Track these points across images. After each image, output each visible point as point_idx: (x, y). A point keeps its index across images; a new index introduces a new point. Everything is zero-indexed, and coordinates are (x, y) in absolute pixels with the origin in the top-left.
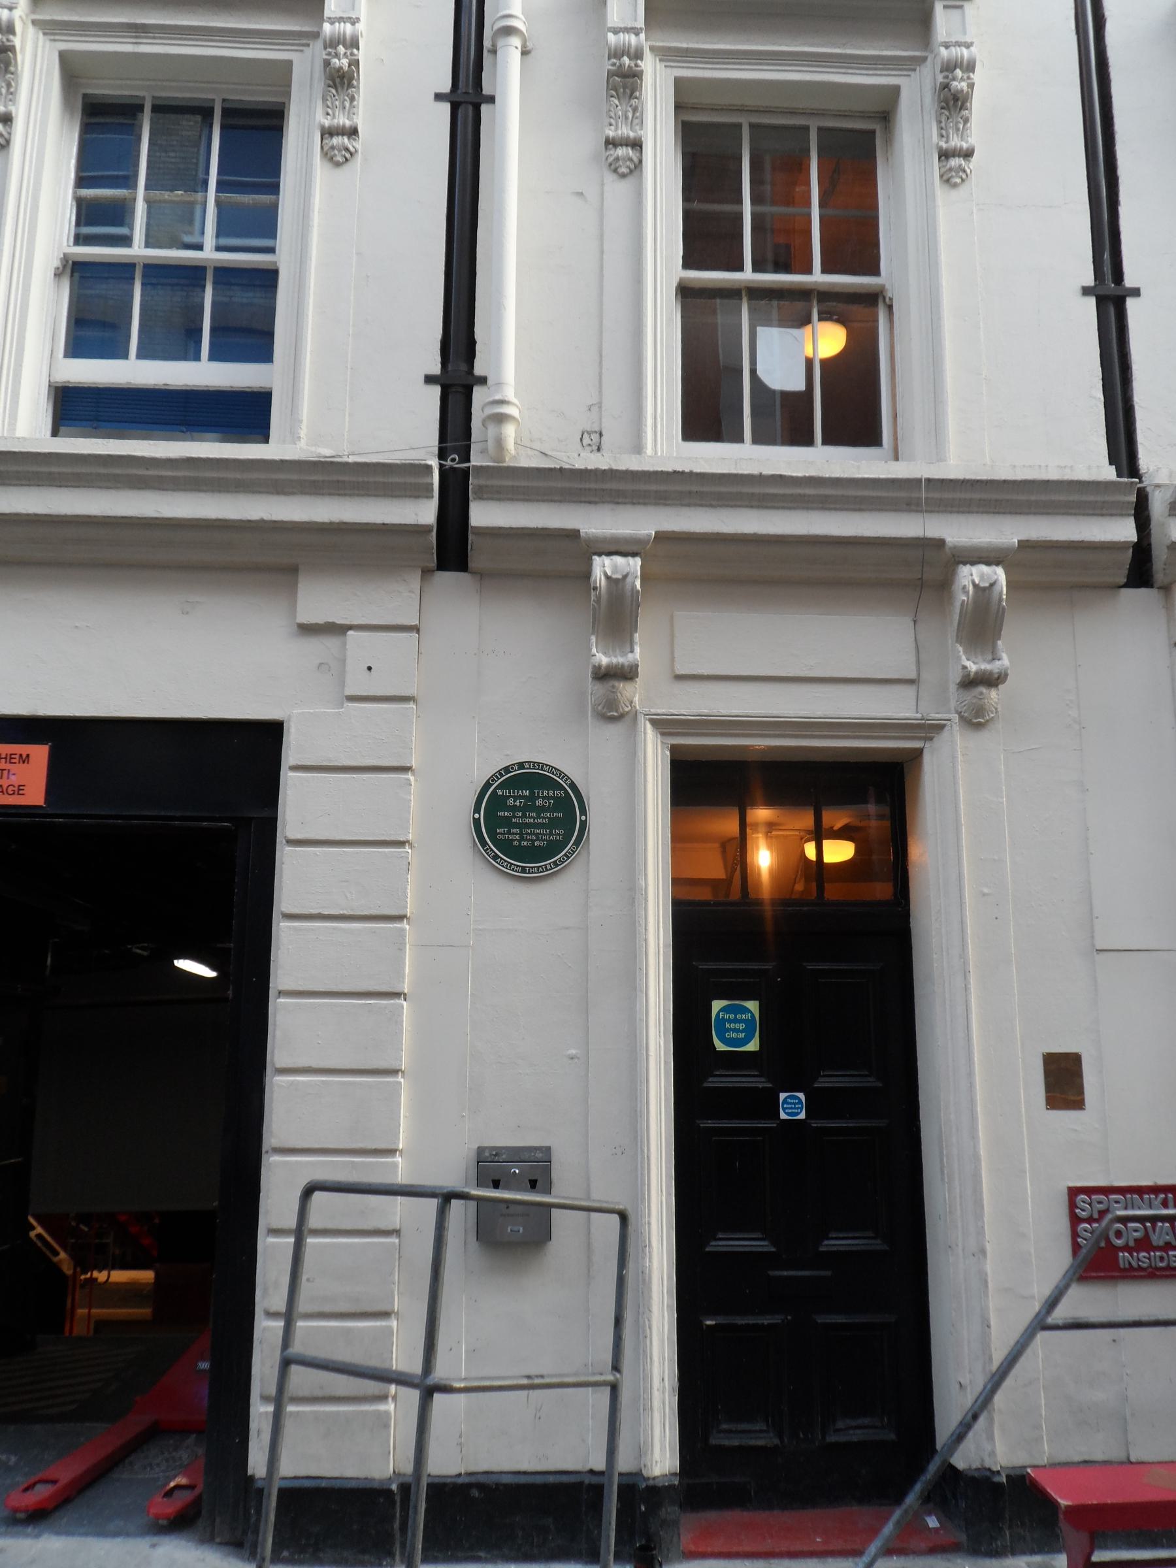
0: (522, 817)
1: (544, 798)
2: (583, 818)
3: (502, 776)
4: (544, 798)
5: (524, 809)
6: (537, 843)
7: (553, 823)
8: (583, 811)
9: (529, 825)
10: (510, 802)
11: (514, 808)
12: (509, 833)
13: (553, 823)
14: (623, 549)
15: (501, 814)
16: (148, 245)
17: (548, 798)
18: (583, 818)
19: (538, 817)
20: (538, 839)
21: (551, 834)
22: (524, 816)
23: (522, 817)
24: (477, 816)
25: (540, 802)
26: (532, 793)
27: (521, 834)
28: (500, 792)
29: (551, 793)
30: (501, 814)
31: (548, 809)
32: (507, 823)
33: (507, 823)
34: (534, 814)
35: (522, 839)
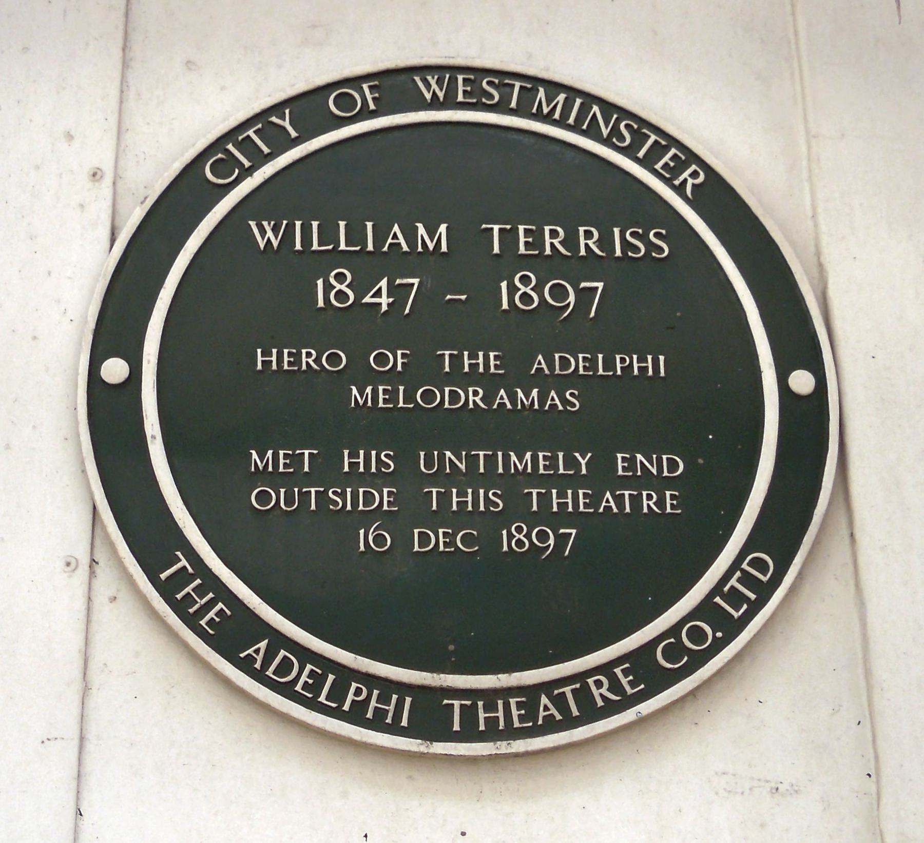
0: (410, 377)
1: (546, 265)
2: (802, 382)
3: (282, 143)
4: (546, 265)
5: (424, 330)
6: (515, 538)
7: (611, 420)
8: (799, 343)
9: (463, 429)
10: (333, 289)
11: (355, 327)
12: (326, 471)
13: (611, 420)
14: (223, 140)
15: (278, 359)
16: (180, 560)
17: (574, 266)
18: (802, 382)
19: (516, 374)
20: (516, 509)
21: (602, 477)
22: (421, 370)
23: (410, 377)
24: (115, 370)
25: (517, 291)
26: (468, 238)
27: (405, 477)
28: (265, 235)
29: (588, 242)
30: (278, 359)
31: (571, 332)
32: (318, 418)
33: (318, 418)
34: (489, 361)
35: (410, 512)
